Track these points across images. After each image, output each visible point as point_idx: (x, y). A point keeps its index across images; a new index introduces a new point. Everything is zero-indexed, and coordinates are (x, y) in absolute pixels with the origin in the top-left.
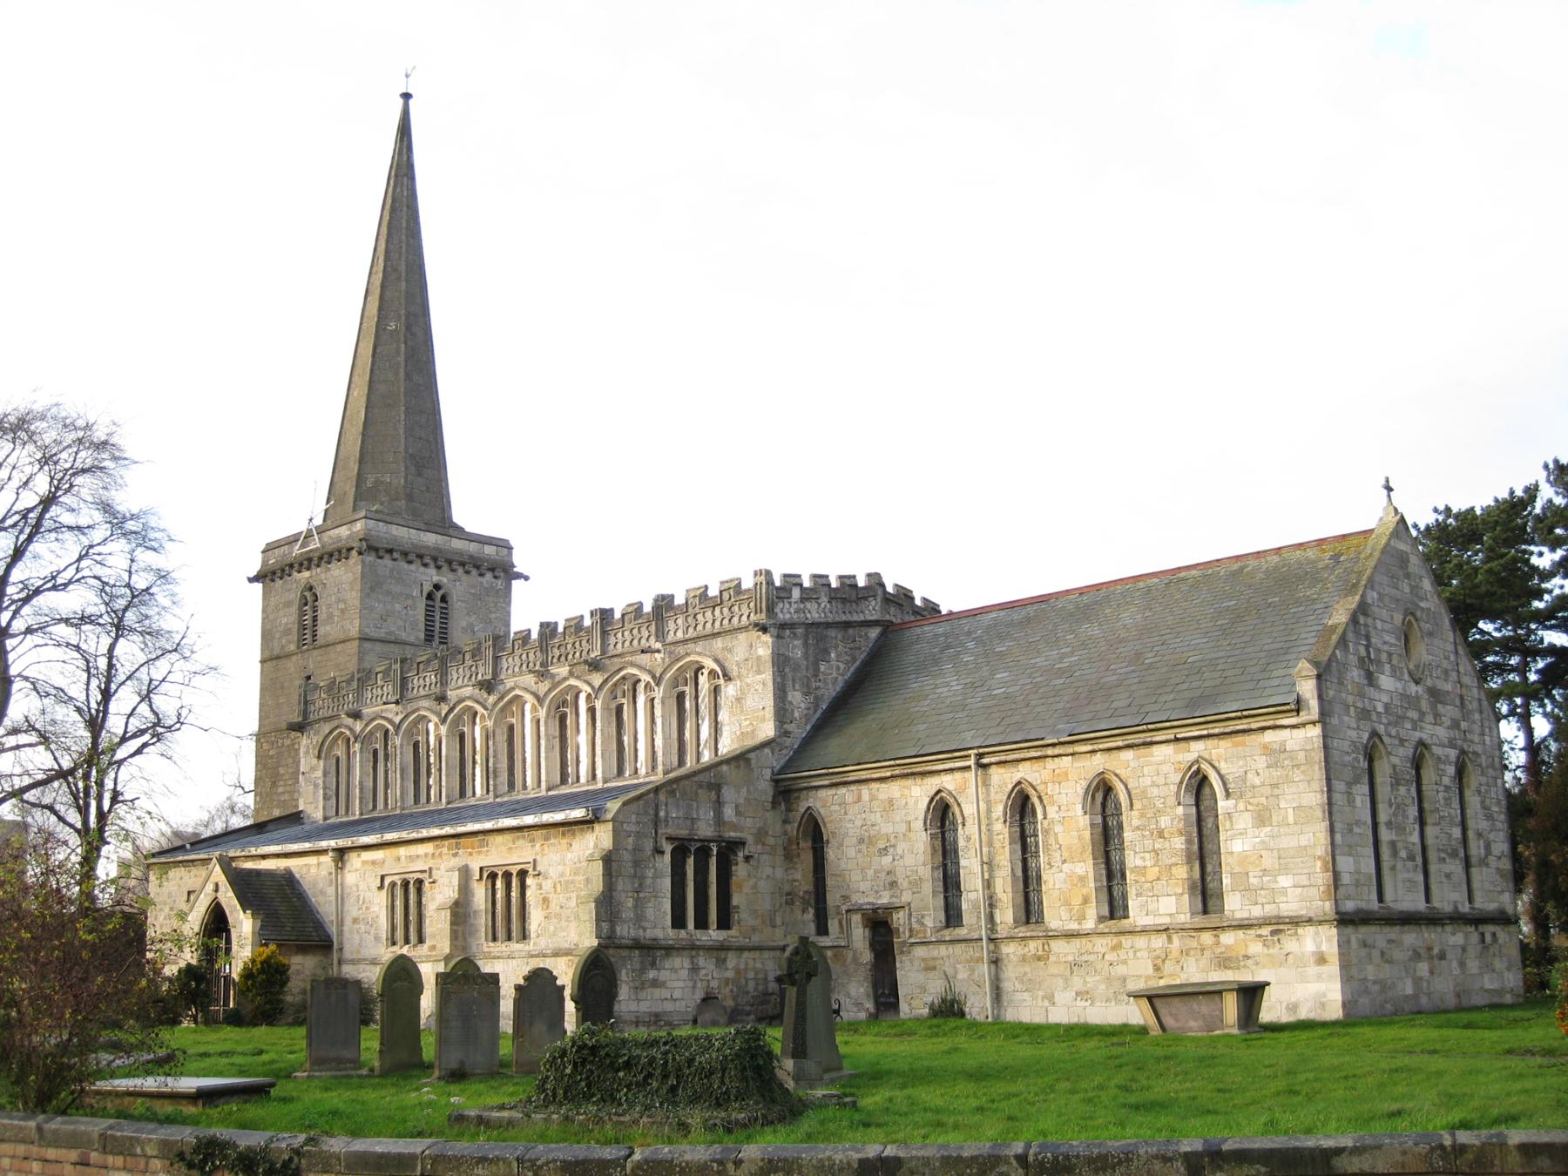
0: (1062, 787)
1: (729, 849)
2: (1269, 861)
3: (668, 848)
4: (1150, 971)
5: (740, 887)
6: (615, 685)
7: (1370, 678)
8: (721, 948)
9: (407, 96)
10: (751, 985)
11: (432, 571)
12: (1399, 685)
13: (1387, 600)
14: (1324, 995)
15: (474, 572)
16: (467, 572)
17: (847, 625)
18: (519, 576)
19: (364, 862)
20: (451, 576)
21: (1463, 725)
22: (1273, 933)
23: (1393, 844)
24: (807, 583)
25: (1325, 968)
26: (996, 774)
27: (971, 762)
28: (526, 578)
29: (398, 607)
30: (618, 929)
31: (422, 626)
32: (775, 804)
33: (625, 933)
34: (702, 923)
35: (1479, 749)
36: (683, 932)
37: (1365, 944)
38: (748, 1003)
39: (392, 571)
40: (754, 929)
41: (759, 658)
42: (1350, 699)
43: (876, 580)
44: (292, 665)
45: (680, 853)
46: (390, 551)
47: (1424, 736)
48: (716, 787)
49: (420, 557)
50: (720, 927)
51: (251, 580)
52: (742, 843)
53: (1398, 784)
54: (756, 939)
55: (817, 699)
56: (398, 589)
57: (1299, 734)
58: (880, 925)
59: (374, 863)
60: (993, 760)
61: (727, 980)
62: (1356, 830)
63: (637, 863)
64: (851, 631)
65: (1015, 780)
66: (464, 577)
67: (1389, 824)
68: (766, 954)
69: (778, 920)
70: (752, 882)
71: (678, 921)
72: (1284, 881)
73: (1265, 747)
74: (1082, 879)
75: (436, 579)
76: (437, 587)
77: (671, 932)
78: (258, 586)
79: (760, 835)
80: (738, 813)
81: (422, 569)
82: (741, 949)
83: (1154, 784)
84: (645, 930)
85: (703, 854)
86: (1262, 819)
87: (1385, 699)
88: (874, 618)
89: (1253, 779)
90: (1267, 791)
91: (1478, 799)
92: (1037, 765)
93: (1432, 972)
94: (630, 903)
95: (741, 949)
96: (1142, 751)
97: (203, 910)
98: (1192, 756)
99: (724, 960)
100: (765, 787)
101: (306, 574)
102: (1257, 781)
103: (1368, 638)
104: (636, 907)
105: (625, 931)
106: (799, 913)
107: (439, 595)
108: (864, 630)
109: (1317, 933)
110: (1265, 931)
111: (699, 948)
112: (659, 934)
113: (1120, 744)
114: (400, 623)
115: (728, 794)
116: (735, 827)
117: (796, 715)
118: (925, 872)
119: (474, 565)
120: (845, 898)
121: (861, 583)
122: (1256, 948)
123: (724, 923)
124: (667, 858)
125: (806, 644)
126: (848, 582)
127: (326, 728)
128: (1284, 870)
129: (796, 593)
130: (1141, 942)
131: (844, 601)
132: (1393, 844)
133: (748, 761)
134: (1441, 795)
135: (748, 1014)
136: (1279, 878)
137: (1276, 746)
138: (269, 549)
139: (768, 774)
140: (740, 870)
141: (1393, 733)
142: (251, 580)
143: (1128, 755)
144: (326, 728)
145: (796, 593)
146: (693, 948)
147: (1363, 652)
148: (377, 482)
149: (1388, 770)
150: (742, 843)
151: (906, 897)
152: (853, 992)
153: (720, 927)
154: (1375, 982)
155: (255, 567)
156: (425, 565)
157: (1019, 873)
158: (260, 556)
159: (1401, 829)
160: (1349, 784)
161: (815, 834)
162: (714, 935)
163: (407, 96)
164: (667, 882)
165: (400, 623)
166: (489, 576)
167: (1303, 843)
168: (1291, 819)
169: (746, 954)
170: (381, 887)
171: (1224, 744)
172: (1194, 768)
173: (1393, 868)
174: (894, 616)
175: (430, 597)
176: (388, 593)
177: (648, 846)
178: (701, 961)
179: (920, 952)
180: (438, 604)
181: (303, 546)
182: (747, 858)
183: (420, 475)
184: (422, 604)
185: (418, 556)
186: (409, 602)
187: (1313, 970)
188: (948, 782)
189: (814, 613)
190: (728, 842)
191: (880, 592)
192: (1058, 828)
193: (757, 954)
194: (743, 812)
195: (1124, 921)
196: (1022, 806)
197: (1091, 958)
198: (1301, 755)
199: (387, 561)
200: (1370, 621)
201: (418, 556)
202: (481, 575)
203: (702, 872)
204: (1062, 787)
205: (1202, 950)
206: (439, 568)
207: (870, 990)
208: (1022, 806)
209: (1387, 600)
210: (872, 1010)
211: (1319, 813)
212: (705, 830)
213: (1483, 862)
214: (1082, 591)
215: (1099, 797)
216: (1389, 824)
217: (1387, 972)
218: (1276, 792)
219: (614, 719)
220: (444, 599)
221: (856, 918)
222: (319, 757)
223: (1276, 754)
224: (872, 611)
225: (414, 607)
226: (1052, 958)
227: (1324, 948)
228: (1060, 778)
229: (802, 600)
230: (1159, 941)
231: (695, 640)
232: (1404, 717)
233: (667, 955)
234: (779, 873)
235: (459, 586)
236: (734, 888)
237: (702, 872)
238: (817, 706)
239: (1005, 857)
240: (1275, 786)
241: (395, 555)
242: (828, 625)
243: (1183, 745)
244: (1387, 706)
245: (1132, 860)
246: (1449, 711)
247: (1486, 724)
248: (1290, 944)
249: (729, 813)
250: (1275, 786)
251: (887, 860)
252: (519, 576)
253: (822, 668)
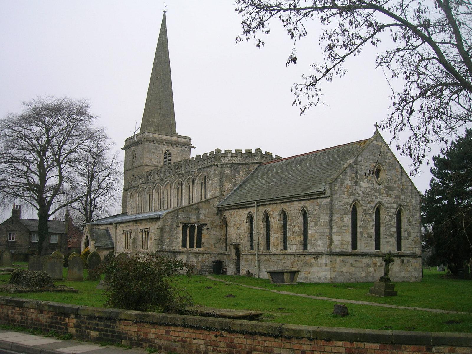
0: (275, 212)
1: (201, 227)
2: (317, 237)
3: (181, 226)
4: (291, 266)
5: (204, 236)
6: (188, 180)
7: (356, 184)
8: (197, 254)
9: (165, 12)
10: (207, 264)
11: (166, 146)
12: (371, 186)
13: (368, 160)
14: (326, 275)
15: (179, 146)
16: (177, 146)
17: (246, 164)
18: (193, 147)
19: (121, 227)
20: (172, 147)
21: (402, 197)
22: (317, 257)
23: (361, 233)
24: (234, 152)
25: (327, 268)
26: (261, 207)
27: (255, 205)
28: (195, 148)
29: (155, 156)
30: (164, 247)
31: (163, 162)
32: (217, 214)
33: (166, 248)
34: (191, 246)
35: (409, 204)
36: (185, 248)
37: (343, 261)
38: (205, 268)
39: (154, 146)
40: (209, 249)
41: (216, 173)
42: (345, 190)
43: (259, 151)
44: (130, 172)
45: (185, 227)
46: (153, 141)
47: (381, 201)
48: (198, 209)
49: (162, 142)
50: (190, 247)
51: (122, 149)
52: (206, 225)
53: (366, 214)
54: (209, 251)
55: (234, 185)
56: (156, 151)
57: (325, 200)
58: (237, 247)
59: (122, 227)
60: (260, 204)
61: (199, 262)
62: (343, 228)
63: (171, 229)
64: (248, 165)
65: (265, 210)
66: (176, 148)
67: (360, 227)
68: (212, 255)
69: (217, 246)
70: (209, 235)
71: (184, 245)
72: (320, 242)
73: (318, 203)
74: (277, 238)
75: (167, 148)
76: (168, 151)
77: (181, 248)
78: (124, 151)
79: (212, 223)
80: (205, 216)
81: (163, 146)
82: (203, 254)
83: (294, 213)
84: (172, 247)
85: (192, 227)
86: (316, 224)
87: (363, 189)
88: (258, 161)
89: (315, 213)
90: (317, 216)
91: (406, 219)
92: (269, 206)
93: (375, 270)
94: (168, 240)
95: (203, 254)
96: (291, 203)
97: (85, 238)
98: (302, 205)
99: (198, 256)
100: (215, 210)
101: (133, 147)
102: (315, 213)
103: (357, 171)
104: (170, 241)
105: (166, 247)
106: (222, 244)
107: (168, 153)
108: (252, 165)
109: (326, 258)
110: (315, 256)
111: (190, 253)
112: (177, 248)
113: (286, 201)
114: (156, 161)
115: (202, 211)
116: (204, 220)
117: (226, 189)
118: (246, 235)
119: (179, 144)
120: (231, 241)
121: (254, 151)
122: (313, 261)
123: (199, 246)
124: (181, 228)
125: (231, 169)
126: (249, 152)
127: (133, 189)
128: (320, 239)
129: (229, 155)
130: (289, 257)
131: (246, 157)
132: (361, 233)
133: (209, 202)
134: (387, 218)
135: (206, 271)
136: (319, 241)
137: (320, 203)
138: (127, 140)
139: (216, 206)
140: (205, 232)
141: (366, 199)
142: (122, 149)
143: (288, 204)
144: (133, 189)
145: (229, 155)
146: (188, 253)
147: (354, 175)
148: (153, 122)
149: (362, 211)
150: (206, 225)
151: (242, 241)
152: (231, 266)
153: (197, 247)
154: (347, 273)
155: (123, 145)
156: (164, 145)
157: (265, 236)
158: (124, 142)
159: (365, 228)
160: (341, 215)
161: (225, 222)
162: (195, 249)
163: (165, 12)
164: (181, 235)
165: (156, 161)
166: (183, 147)
167: (324, 231)
168: (322, 225)
169: (205, 255)
170: (123, 234)
171: (309, 202)
172: (302, 209)
173: (360, 240)
174: (264, 161)
175: (165, 153)
176: (153, 153)
177: (175, 225)
178: (190, 256)
179: (245, 257)
180: (168, 155)
181: (133, 140)
182: (207, 229)
183: (165, 119)
184: (163, 156)
185: (163, 142)
186: (159, 155)
187: (325, 268)
188: (251, 210)
189: (235, 160)
190: (201, 224)
191: (260, 154)
192: (273, 224)
193: (209, 255)
194: (206, 215)
195: (286, 251)
196: (267, 217)
197: (279, 261)
198: (325, 206)
199: (152, 144)
200: (359, 166)
201: (163, 142)
202: (181, 147)
203: (192, 232)
204: (275, 212)
205: (302, 260)
206: (168, 145)
207: (235, 266)
208: (267, 217)
209: (368, 160)
210: (235, 272)
211: (328, 223)
212: (194, 220)
213: (407, 238)
214: (303, 155)
215: (282, 215)
216: (360, 227)
217: (353, 269)
218: (320, 216)
219: (188, 189)
220: (170, 154)
221: (232, 246)
222: (131, 198)
223: (320, 205)
224: (257, 159)
225: (160, 156)
226: (271, 260)
227: (327, 262)
228: (274, 210)
229: (231, 157)
230: (293, 257)
231: (203, 168)
232: (372, 195)
233: (179, 254)
234: (218, 233)
235: (174, 151)
236: (203, 237)
237: (192, 232)
238: (234, 187)
239: (263, 231)
240: (319, 214)
241: (154, 142)
242: (239, 164)
243: (300, 202)
244: (363, 192)
245: (289, 234)
246: (394, 193)
247: (414, 196)
248: (320, 260)
249: (202, 216)
250: (319, 214)
251: (239, 231)
252: (193, 147)
253: (237, 176)
